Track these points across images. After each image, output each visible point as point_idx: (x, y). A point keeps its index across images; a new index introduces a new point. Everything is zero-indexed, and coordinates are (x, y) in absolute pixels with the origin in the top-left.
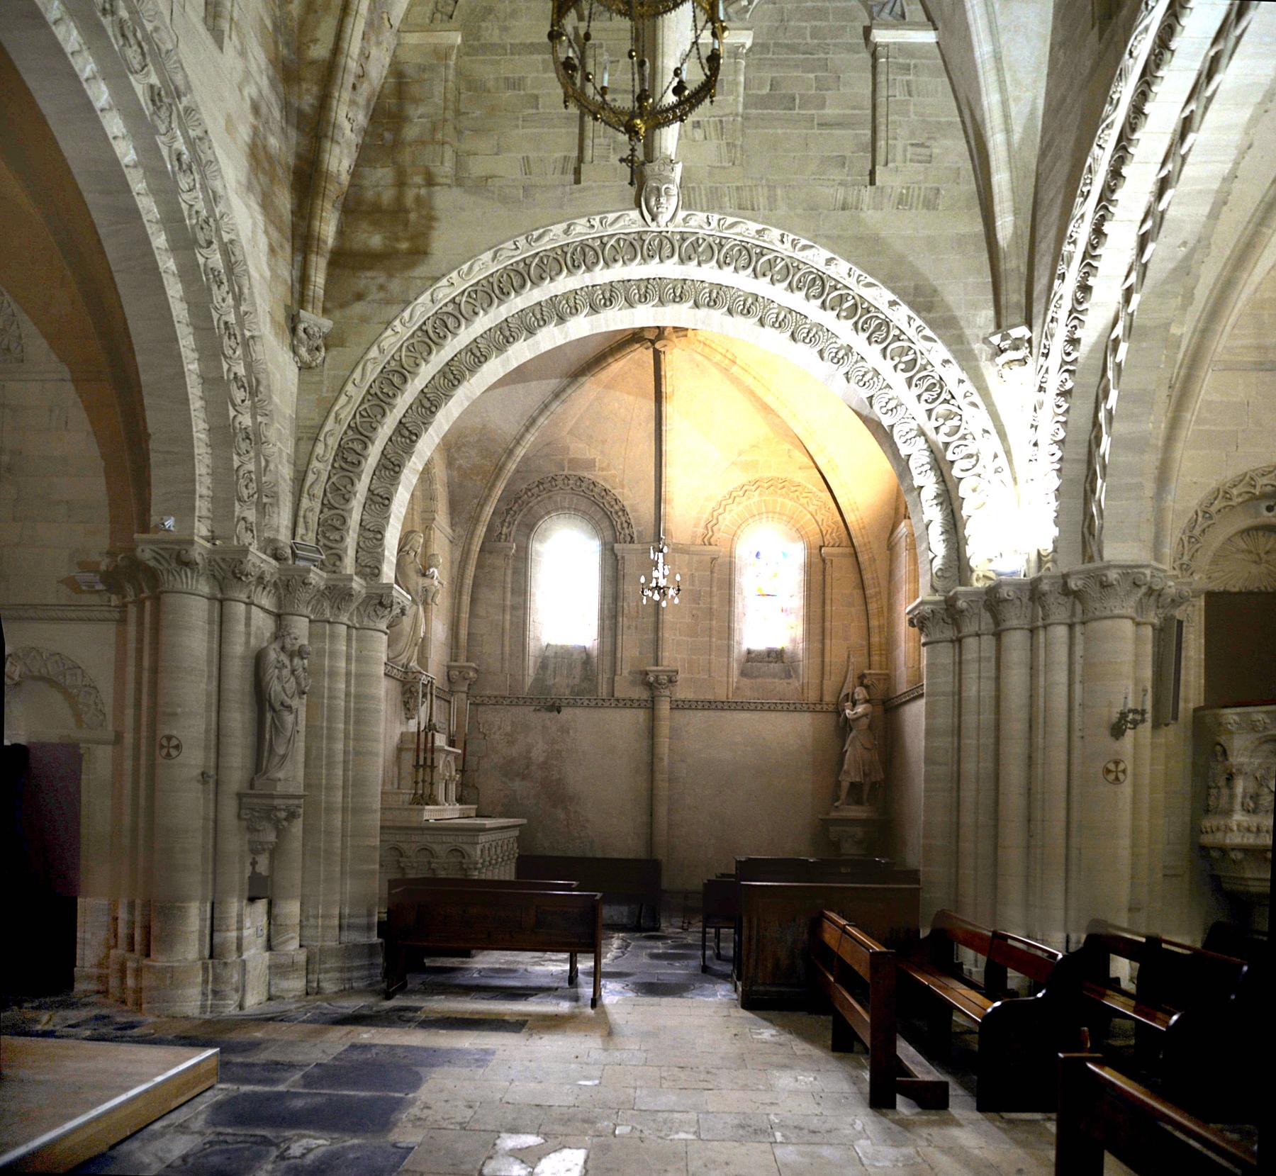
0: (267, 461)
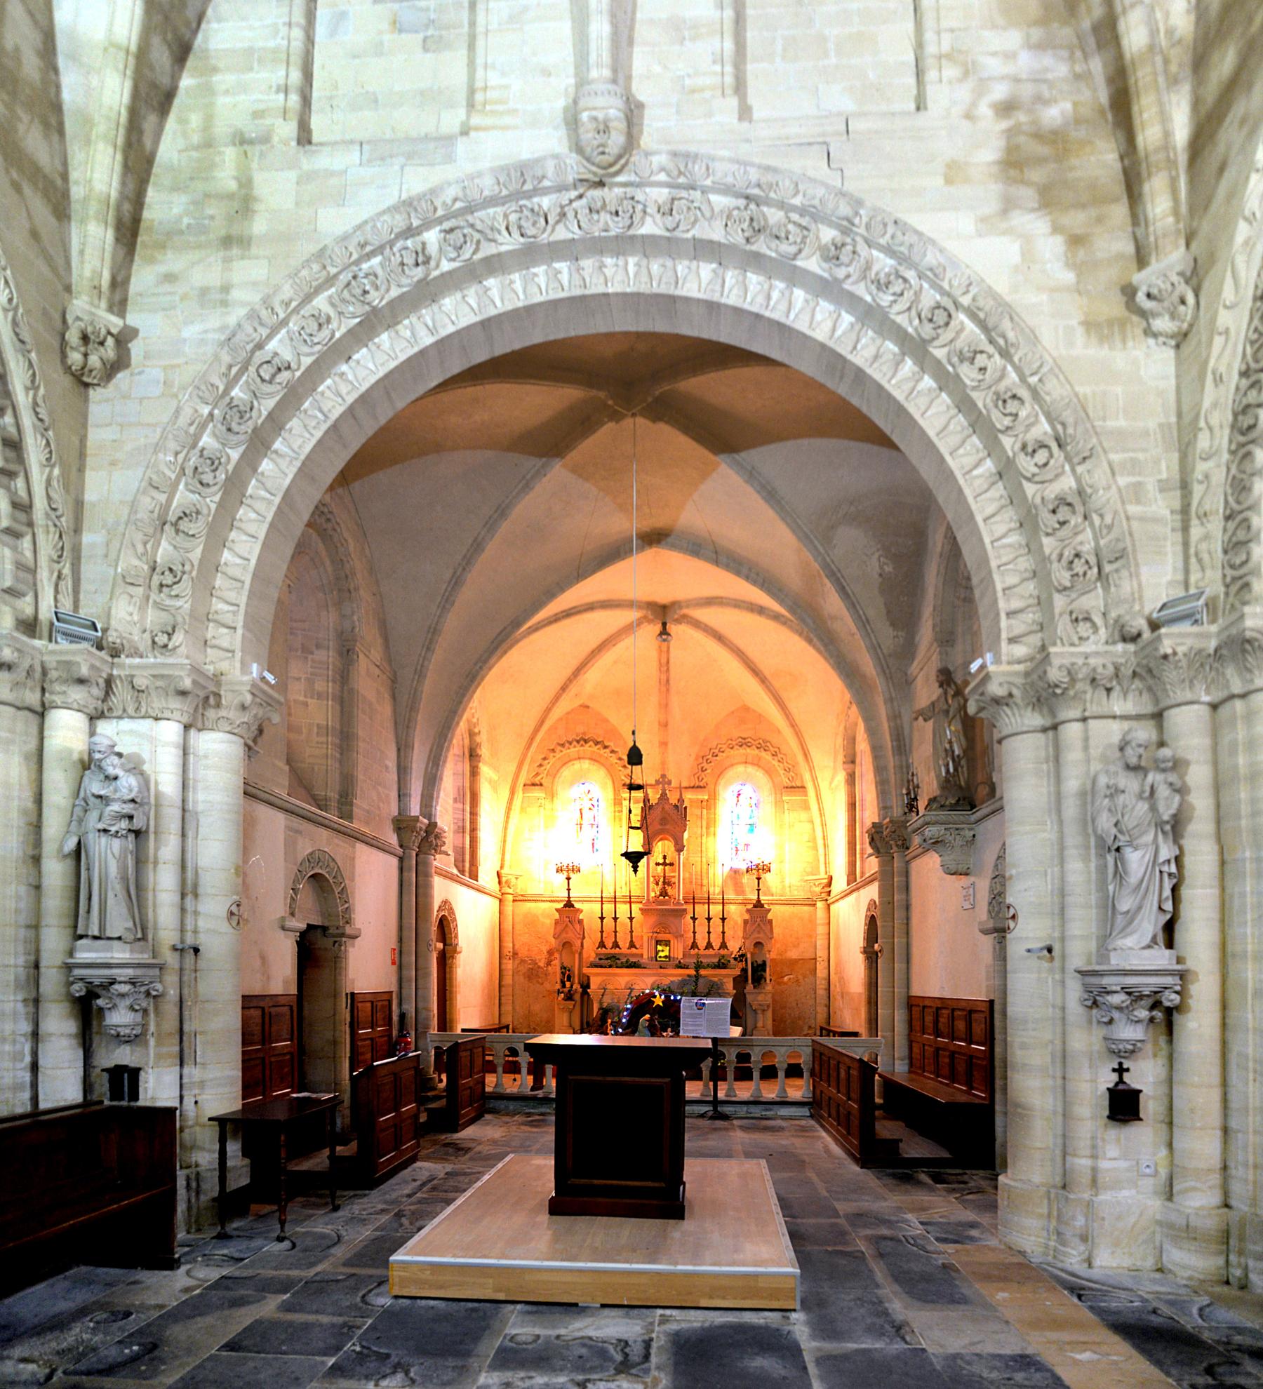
0: (1102, 516)
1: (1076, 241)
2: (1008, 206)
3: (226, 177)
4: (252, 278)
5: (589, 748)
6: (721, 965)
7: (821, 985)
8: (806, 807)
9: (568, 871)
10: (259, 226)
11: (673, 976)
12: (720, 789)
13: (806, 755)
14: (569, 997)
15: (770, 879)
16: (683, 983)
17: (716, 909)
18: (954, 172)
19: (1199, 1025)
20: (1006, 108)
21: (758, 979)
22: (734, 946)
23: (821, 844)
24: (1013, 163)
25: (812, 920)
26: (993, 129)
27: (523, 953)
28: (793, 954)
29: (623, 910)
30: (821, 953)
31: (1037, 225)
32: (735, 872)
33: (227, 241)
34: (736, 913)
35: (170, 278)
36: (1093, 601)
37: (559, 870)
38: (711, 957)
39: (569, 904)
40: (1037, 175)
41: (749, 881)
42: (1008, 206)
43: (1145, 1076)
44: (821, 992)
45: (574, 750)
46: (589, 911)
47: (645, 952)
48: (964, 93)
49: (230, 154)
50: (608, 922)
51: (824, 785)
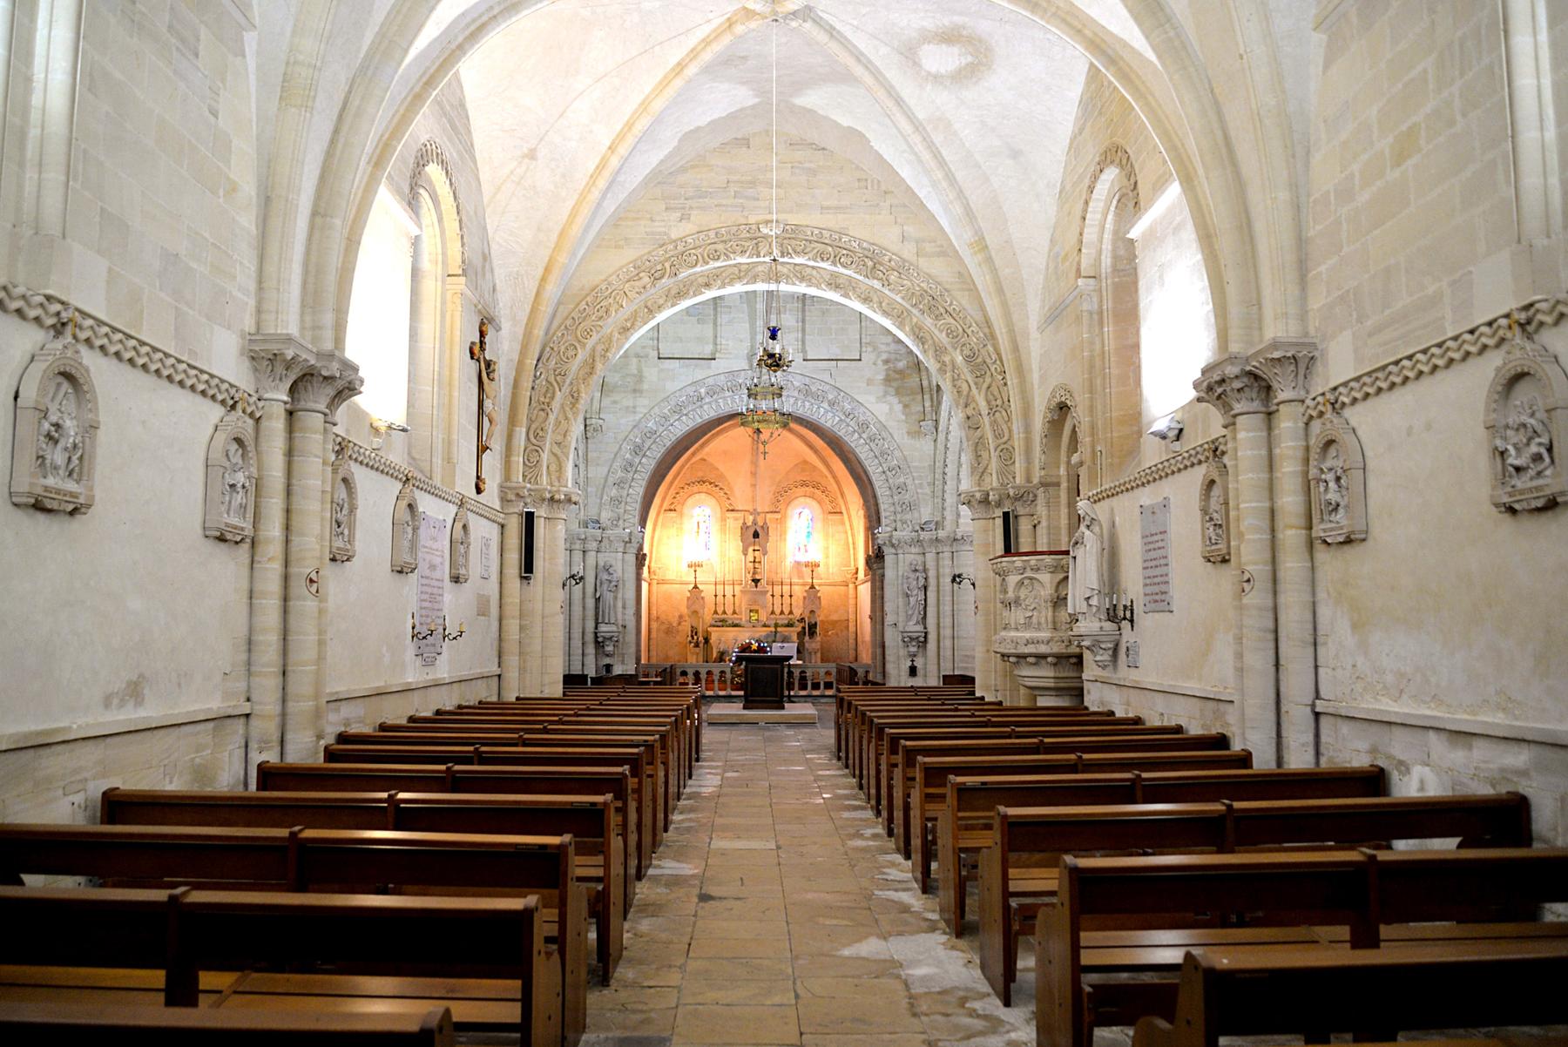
1: (906, 406)
2: (886, 393)
3: (633, 369)
4: (643, 403)
5: (706, 487)
6: (790, 625)
7: (852, 636)
8: (843, 523)
9: (695, 566)
10: (645, 386)
11: (762, 632)
12: (789, 512)
13: (842, 494)
14: (697, 645)
15: (821, 570)
16: (767, 636)
17: (786, 588)
18: (869, 382)
19: (932, 645)
20: (886, 362)
21: (812, 633)
22: (797, 613)
23: (848, 547)
24: (888, 380)
25: (846, 596)
26: (882, 367)
27: (663, 617)
28: (835, 617)
29: (729, 589)
30: (852, 617)
31: (895, 400)
32: (798, 563)
33: (635, 391)
34: (799, 591)
35: (615, 402)
36: (908, 517)
37: (690, 566)
38: (783, 620)
39: (696, 587)
40: (895, 384)
41: (807, 571)
42: (886, 393)
43: (919, 663)
44: (852, 641)
45: (695, 488)
46: (708, 591)
47: (744, 618)
48: (873, 356)
49: (635, 360)
50: (720, 598)
51: (853, 513)
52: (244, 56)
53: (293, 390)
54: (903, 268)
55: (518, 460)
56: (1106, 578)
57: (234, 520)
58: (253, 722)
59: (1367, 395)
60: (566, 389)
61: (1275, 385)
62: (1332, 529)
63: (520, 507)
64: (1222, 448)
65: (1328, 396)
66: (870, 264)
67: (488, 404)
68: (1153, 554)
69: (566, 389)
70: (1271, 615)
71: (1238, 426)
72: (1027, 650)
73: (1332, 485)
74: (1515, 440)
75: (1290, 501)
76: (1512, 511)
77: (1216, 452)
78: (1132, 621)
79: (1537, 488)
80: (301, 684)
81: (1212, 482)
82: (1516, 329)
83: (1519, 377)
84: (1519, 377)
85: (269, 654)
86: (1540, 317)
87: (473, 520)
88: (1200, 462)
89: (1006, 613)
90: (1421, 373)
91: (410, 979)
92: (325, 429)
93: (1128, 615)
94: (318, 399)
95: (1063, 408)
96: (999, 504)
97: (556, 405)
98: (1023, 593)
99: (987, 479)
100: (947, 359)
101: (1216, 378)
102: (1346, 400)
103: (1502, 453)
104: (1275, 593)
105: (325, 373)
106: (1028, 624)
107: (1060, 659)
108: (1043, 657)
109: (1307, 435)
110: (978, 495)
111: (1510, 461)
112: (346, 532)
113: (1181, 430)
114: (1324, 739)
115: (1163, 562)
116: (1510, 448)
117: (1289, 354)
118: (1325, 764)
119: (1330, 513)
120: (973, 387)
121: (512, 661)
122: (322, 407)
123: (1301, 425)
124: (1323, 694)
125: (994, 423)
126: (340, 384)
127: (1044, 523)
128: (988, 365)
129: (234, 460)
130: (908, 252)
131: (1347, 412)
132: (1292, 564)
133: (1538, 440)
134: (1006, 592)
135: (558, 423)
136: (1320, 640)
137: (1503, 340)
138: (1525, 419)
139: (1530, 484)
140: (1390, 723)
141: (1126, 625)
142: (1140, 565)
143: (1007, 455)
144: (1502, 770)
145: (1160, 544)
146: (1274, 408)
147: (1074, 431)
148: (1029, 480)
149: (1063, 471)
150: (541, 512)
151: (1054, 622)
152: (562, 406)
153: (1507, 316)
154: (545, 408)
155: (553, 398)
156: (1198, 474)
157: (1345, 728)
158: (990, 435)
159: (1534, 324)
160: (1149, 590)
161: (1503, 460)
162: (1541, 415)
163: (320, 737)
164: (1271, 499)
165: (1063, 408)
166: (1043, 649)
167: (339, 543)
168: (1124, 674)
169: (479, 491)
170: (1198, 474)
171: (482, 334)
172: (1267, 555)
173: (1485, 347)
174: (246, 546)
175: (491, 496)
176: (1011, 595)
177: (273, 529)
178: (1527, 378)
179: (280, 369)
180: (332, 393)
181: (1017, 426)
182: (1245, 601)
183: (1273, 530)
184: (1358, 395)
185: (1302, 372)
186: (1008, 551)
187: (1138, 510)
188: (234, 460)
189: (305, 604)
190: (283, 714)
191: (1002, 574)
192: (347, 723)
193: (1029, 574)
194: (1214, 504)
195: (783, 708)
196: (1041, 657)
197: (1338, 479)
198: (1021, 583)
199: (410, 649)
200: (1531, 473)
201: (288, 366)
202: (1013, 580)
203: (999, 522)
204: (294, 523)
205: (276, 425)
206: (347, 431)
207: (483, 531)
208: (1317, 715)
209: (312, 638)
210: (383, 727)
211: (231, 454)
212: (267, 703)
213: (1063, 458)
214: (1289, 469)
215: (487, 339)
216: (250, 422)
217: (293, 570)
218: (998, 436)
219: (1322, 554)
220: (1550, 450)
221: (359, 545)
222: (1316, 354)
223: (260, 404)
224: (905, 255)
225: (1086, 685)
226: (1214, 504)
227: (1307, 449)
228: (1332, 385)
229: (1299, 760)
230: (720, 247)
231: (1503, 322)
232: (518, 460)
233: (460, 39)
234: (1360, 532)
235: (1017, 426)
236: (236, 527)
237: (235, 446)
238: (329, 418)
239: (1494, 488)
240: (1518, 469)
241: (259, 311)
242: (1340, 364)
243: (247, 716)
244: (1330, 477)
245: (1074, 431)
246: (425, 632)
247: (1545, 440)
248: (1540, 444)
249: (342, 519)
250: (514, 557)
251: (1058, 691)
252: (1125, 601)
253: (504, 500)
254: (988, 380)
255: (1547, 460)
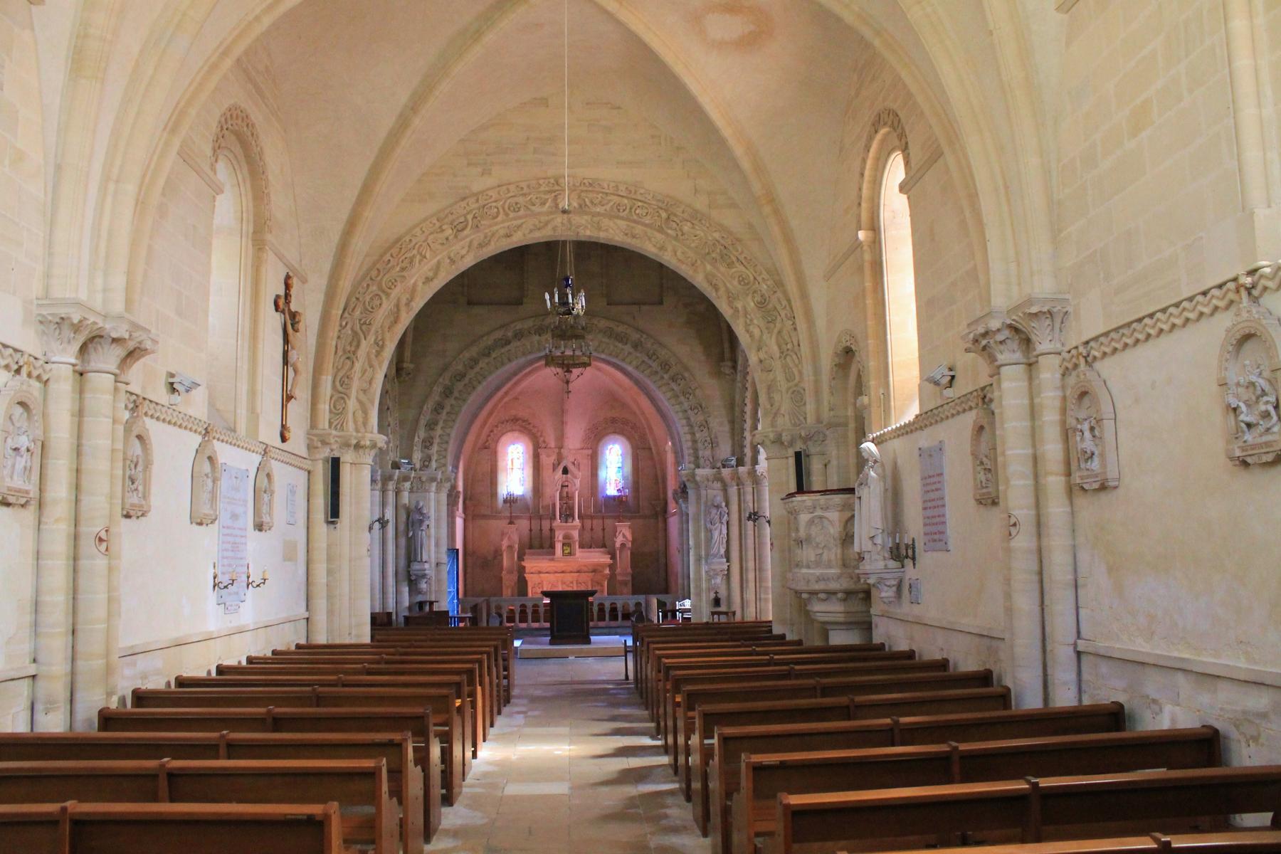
52: (33, 29)
53: (83, 349)
54: (696, 217)
55: (324, 408)
56: (890, 515)
57: (18, 482)
58: (40, 683)
59: (1115, 350)
60: (371, 338)
61: (1033, 337)
62: (1088, 477)
63: (325, 453)
64: (989, 395)
65: (1081, 349)
66: (664, 215)
67: (293, 355)
68: (932, 495)
69: (371, 338)
70: (1035, 558)
71: (1002, 376)
72: (817, 587)
73: (1087, 434)
74: (1245, 397)
75: (1053, 449)
76: (1245, 464)
77: (984, 398)
78: (914, 559)
79: (1267, 444)
80: (92, 643)
81: (982, 428)
82: (1244, 293)
83: (1248, 337)
84: (1248, 337)
85: (56, 615)
86: (1263, 282)
87: (276, 467)
88: (971, 408)
89: (799, 551)
90: (1161, 330)
91: (916, 354)
92: (116, 389)
93: (910, 552)
94: (107, 359)
95: (849, 352)
96: (791, 443)
97: (362, 352)
98: (814, 530)
99: (780, 421)
100: (739, 305)
101: (981, 330)
102: (1096, 354)
103: (1235, 409)
104: (1039, 535)
105: (114, 335)
106: (818, 564)
107: (849, 594)
108: (834, 593)
109: (1063, 387)
110: (772, 436)
111: (1242, 417)
112: (140, 488)
113: (953, 377)
114: (1085, 676)
115: (940, 503)
116: (1241, 404)
117: (1045, 309)
118: (1086, 701)
119: (1086, 461)
120: (765, 331)
121: (321, 604)
122: (113, 367)
123: (1058, 376)
124: (1084, 633)
125: (785, 367)
126: (131, 345)
127: (834, 463)
128: (528, 508)
129: (17, 425)
130: (700, 203)
131: (1097, 365)
132: (1056, 508)
133: (1265, 399)
134: (797, 530)
135: (364, 372)
136: (1080, 582)
137: (1232, 302)
138: (1254, 378)
139: (1259, 440)
140: (1143, 664)
141: (908, 562)
142: (920, 506)
143: (797, 396)
144: (1244, 712)
145: (938, 486)
146: (1033, 360)
147: (859, 376)
148: (819, 421)
149: (850, 412)
150: (347, 458)
151: (843, 560)
152: (368, 354)
153: (1235, 280)
154: (350, 356)
155: (358, 346)
156: (969, 419)
157: (1104, 668)
158: (780, 377)
159: (1260, 287)
160: (929, 529)
161: (1236, 416)
162: (1266, 374)
163: (109, 694)
164: (1034, 446)
165: (849, 352)
166: (833, 586)
167: (134, 499)
168: (906, 609)
169: (284, 439)
170: (969, 419)
171: (288, 286)
172: (1032, 500)
173: (1216, 308)
174: (32, 508)
175: (298, 442)
176: (802, 534)
177: (59, 490)
178: (1254, 339)
179: (67, 333)
180: (124, 354)
181: (807, 370)
182: (1013, 544)
183: (1036, 476)
184: (1108, 350)
185: (1057, 325)
186: (801, 490)
187: (916, 452)
188: (17, 425)
189: (95, 563)
190: (73, 673)
191: (793, 513)
192: (144, 677)
193: (819, 513)
194: (984, 448)
195: (589, 642)
196: (831, 593)
197: (1092, 429)
198: (811, 522)
199: (212, 597)
200: (1261, 429)
201: (76, 328)
202: (804, 518)
203: (792, 461)
204: (85, 483)
205: (63, 387)
206: (144, 388)
207: (287, 479)
208: (1079, 654)
209: (102, 597)
210: (181, 682)
211: (15, 418)
212: (57, 666)
213: (851, 400)
214: (1050, 417)
215: (293, 292)
216: (37, 384)
217: (83, 529)
218: (789, 379)
219: (1081, 501)
220: (1276, 407)
221: (155, 500)
222: (1070, 309)
223: (48, 367)
224: (698, 206)
225: (875, 620)
226: (984, 448)
227: (1064, 399)
228: (1084, 339)
229: (1065, 698)
230: (521, 200)
231: (1231, 285)
232: (324, 408)
233: (258, 11)
234: (1114, 480)
235: (807, 370)
236: (19, 491)
237: (19, 410)
238: (122, 378)
239: (1228, 442)
240: (1249, 425)
241: (48, 276)
242: (1091, 320)
243: (34, 677)
244: (1086, 427)
245: (859, 376)
246: (225, 579)
247: (1272, 399)
248: (1267, 402)
249: (135, 473)
250: (320, 503)
251: (848, 625)
252: (907, 540)
253: (311, 447)
254: (778, 325)
255: (1275, 418)
